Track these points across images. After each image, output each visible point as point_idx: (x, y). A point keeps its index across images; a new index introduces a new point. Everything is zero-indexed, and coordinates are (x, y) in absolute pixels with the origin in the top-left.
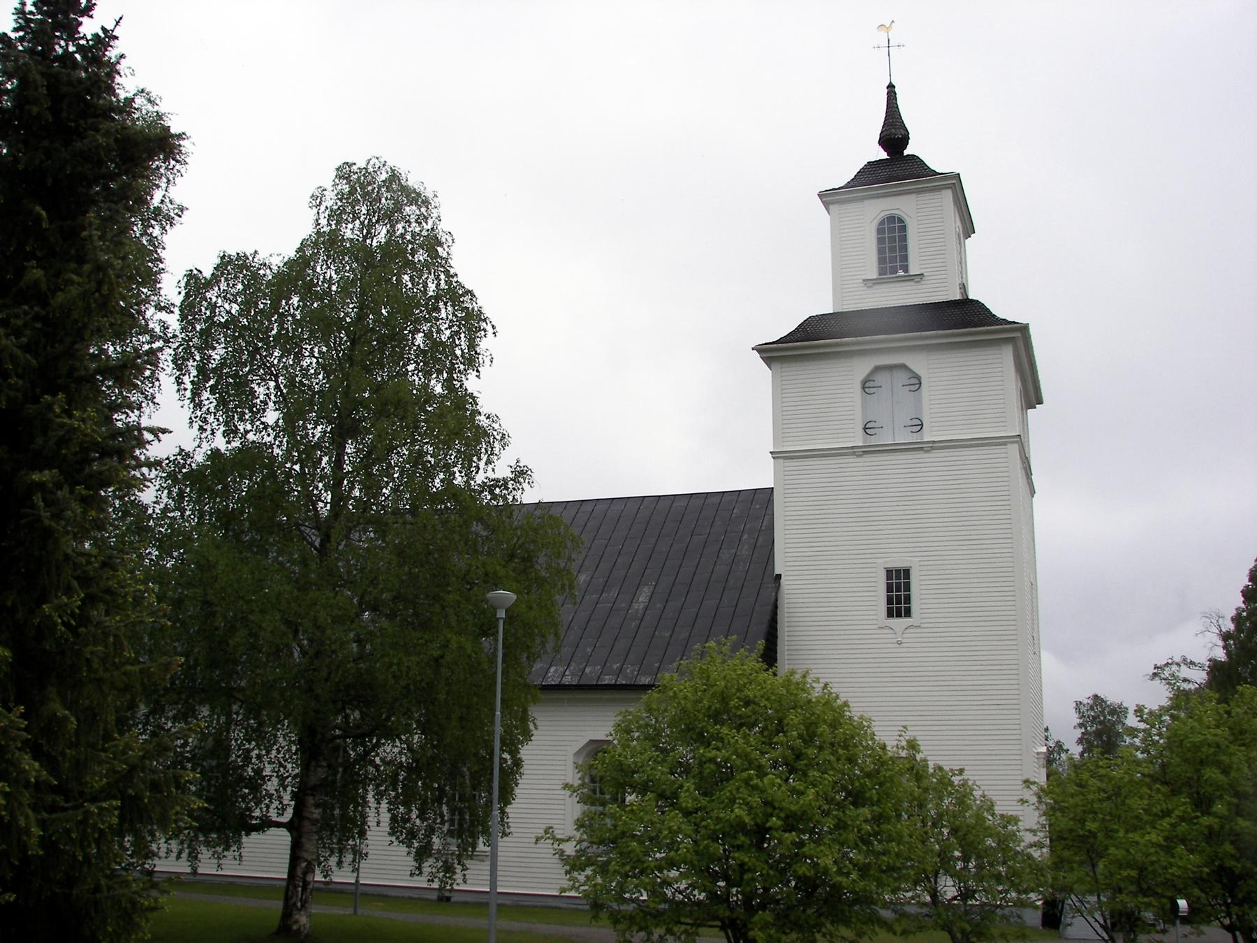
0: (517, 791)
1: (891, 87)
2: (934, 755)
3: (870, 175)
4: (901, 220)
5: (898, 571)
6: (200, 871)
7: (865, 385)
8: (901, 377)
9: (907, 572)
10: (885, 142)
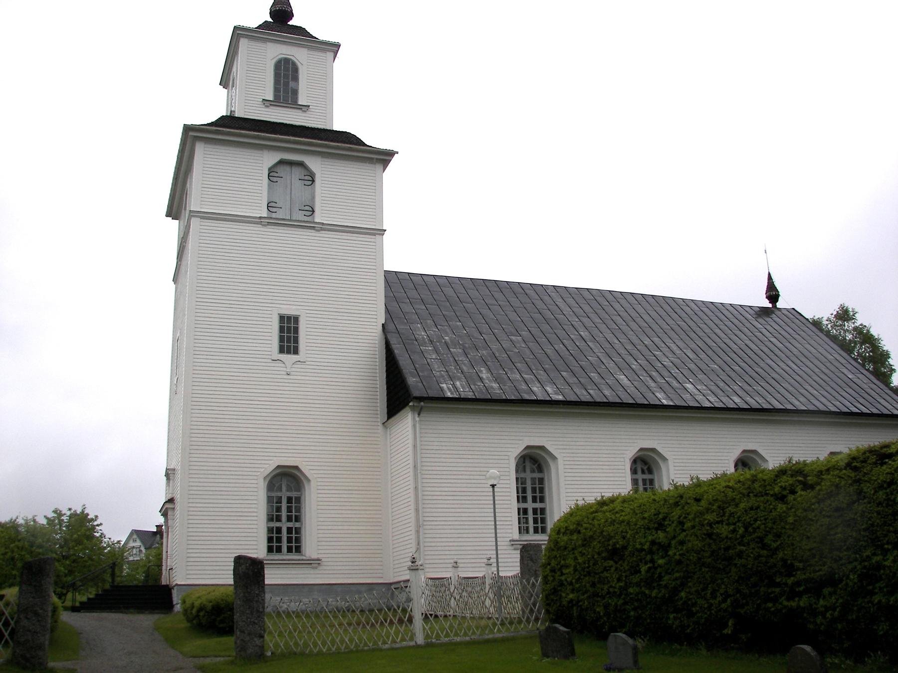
0: (591, 500)
2: (705, 476)
4: (294, 64)
5: (289, 318)
6: (193, 220)
7: (271, 170)
8: (297, 172)
9: (296, 319)
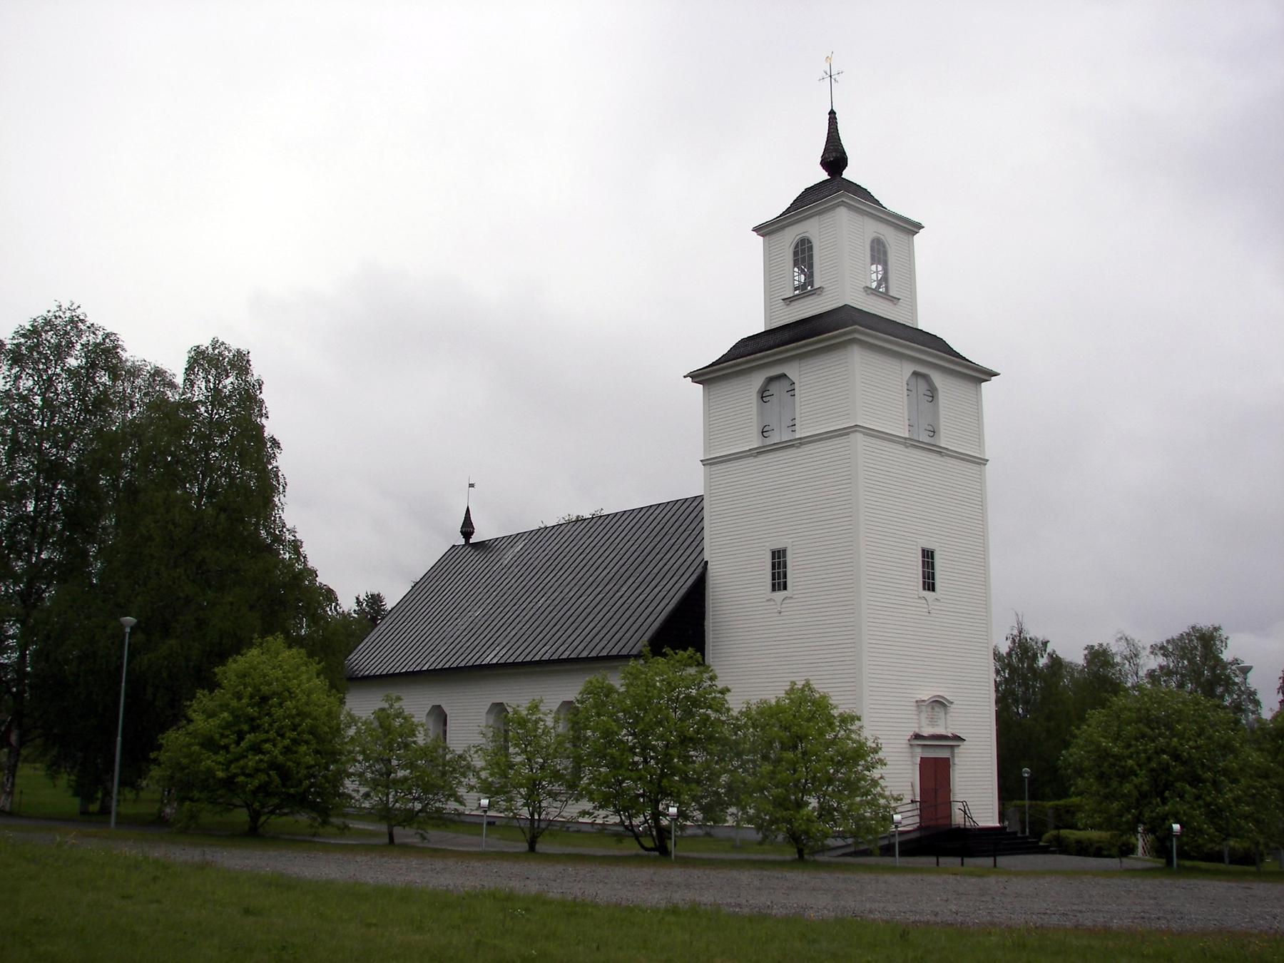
1: (832, 113)
3: (809, 200)
7: (763, 395)
10: (825, 164)
